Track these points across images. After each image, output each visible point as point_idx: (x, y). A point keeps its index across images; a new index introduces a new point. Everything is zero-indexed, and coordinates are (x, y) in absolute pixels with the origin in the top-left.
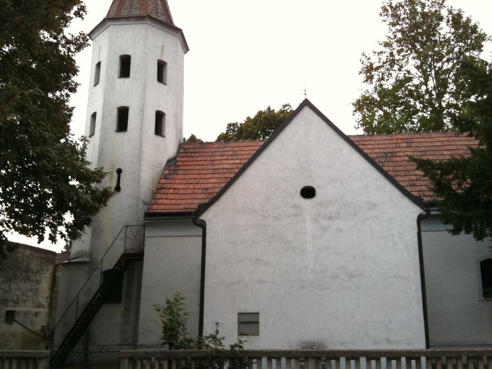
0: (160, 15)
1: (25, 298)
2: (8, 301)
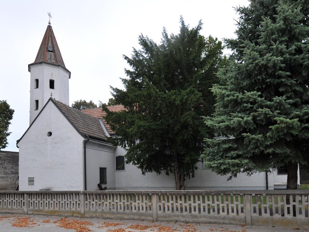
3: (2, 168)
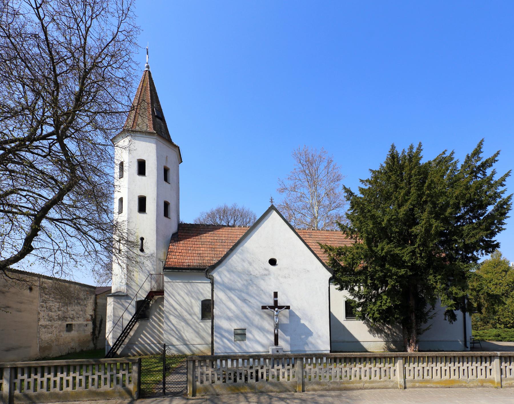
0: (163, 134)
1: (78, 316)
2: (67, 318)
3: (45, 309)
